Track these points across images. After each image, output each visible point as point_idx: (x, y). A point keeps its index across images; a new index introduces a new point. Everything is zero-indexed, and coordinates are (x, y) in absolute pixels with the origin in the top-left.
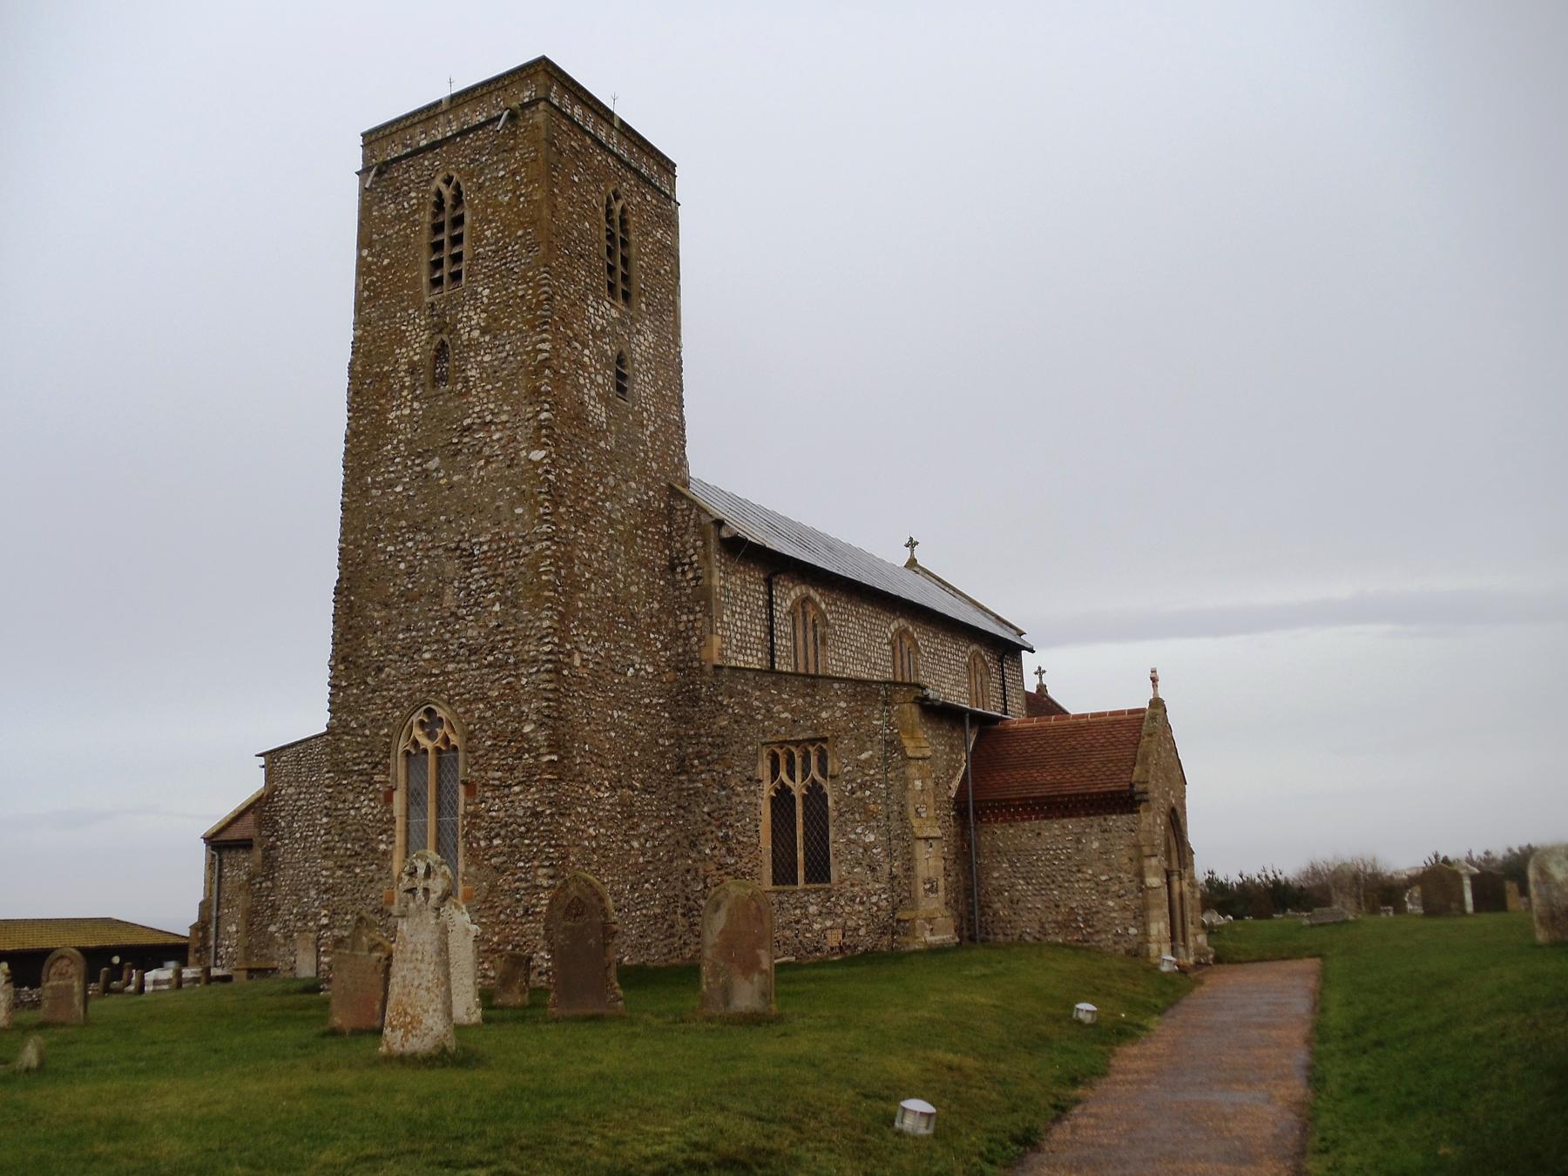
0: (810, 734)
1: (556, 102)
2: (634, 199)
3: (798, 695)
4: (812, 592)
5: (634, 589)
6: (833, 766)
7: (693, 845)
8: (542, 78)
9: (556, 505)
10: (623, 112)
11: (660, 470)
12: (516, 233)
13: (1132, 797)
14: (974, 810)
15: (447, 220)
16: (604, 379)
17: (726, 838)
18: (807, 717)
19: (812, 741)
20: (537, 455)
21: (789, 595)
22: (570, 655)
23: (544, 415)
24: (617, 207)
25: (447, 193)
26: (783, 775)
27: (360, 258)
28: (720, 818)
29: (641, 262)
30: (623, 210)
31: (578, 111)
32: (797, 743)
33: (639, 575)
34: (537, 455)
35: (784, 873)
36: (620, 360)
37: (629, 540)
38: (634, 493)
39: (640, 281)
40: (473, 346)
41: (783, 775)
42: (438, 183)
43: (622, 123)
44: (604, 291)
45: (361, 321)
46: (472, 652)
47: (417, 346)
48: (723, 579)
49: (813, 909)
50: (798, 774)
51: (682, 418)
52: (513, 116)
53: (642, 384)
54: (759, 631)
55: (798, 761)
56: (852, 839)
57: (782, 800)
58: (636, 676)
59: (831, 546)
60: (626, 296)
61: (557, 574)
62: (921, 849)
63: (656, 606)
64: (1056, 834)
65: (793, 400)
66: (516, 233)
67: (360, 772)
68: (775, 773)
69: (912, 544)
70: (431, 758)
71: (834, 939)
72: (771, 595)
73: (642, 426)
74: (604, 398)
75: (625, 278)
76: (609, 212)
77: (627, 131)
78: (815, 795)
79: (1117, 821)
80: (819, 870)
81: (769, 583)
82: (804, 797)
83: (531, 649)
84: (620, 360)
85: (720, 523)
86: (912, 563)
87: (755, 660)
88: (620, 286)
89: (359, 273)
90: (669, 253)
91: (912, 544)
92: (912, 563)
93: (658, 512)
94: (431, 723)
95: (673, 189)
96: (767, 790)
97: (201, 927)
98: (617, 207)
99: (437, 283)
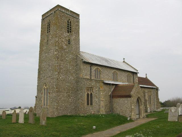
0: (91, 87)
1: (60, 10)
2: (72, 19)
3: (89, 82)
4: (98, 67)
5: (71, 68)
6: (93, 91)
7: (79, 100)
8: (58, 7)
9: (58, 59)
10: (71, 9)
11: (75, 53)
12: (61, 25)
13: (130, 96)
14: (113, 96)
15: (49, 26)
16: (66, 43)
17: (82, 99)
18: (90, 84)
19: (91, 87)
20: (56, 53)
21: (94, 68)
22: (60, 77)
23: (57, 48)
24: (69, 21)
25: (49, 21)
26: (88, 92)
27: (41, 30)
28: (81, 97)
29: (73, 28)
30: (70, 21)
31: (63, 10)
32: (90, 88)
33: (71, 66)
34: (56, 53)
35: (88, 104)
36: (69, 40)
37: (70, 63)
38: (71, 56)
39: (73, 29)
40: (50, 40)
41: (88, 92)
42: (48, 21)
43: (71, 11)
44: (67, 32)
45: (41, 38)
46: (50, 77)
47: (46, 41)
48: (82, 66)
49: (91, 109)
51: (79, 46)
52: (55, 12)
53: (72, 42)
54: (89, 73)
55: (90, 90)
56: (95, 100)
57: (88, 94)
58: (71, 79)
59: (106, 60)
60: (70, 32)
61: (58, 67)
62: (102, 102)
63: (74, 70)
64: (122, 100)
65: (96, 42)
66: (61, 25)
67: (40, 91)
68: (87, 91)
69: (124, 59)
70: (46, 89)
71: (93, 112)
72: (91, 68)
73: (72, 48)
74: (66, 45)
75: (70, 29)
76: (68, 22)
77: (71, 11)
78: (91, 94)
79: (129, 99)
80: (91, 104)
81: (91, 66)
82: (90, 95)
83: (55, 77)
84: (69, 40)
85: (82, 60)
86: (124, 62)
87: (88, 77)
88: (69, 30)
89: (41, 32)
90: (78, 26)
91: (124, 59)
92: (124, 62)
93: (75, 59)
94: (46, 86)
95: (79, 17)
96: (86, 93)
97: (168, 122)
98: (69, 21)
99: (48, 32)
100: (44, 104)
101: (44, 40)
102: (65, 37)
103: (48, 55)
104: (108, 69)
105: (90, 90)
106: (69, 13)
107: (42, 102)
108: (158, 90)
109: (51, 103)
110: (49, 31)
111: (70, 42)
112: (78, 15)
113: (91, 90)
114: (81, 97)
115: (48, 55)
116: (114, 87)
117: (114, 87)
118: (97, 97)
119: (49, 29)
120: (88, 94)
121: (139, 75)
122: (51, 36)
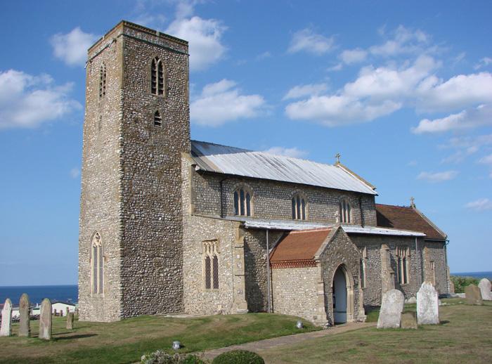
0: (214, 238)
1: (128, 34)
4: (245, 184)
24: (157, 63)
26: (208, 252)
30: (160, 62)
31: (139, 35)
35: (208, 286)
36: (157, 113)
40: (106, 116)
41: (208, 252)
49: (215, 298)
50: (211, 251)
55: (211, 247)
57: (208, 260)
71: (220, 308)
75: (102, 71)
76: (153, 65)
78: (216, 259)
80: (216, 286)
81: (221, 183)
91: (413, 200)
96: (203, 257)
98: (157, 63)
100: (404, 260)
101: (93, 116)
102: (144, 107)
103: (103, 156)
104: (278, 187)
105: (211, 247)
106: (157, 41)
107: (90, 282)
108: (447, 242)
109: (111, 283)
110: (104, 93)
111: (159, 120)
112: (187, 43)
113: (215, 247)
114: (193, 265)
115: (103, 156)
116: (281, 234)
117: (281, 234)
118: (228, 267)
119: (105, 87)
120: (208, 257)
121: (459, 259)
122: (107, 107)
